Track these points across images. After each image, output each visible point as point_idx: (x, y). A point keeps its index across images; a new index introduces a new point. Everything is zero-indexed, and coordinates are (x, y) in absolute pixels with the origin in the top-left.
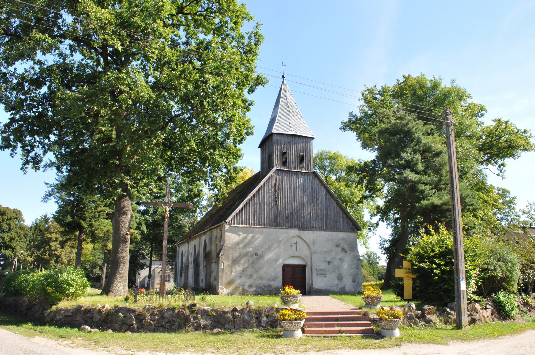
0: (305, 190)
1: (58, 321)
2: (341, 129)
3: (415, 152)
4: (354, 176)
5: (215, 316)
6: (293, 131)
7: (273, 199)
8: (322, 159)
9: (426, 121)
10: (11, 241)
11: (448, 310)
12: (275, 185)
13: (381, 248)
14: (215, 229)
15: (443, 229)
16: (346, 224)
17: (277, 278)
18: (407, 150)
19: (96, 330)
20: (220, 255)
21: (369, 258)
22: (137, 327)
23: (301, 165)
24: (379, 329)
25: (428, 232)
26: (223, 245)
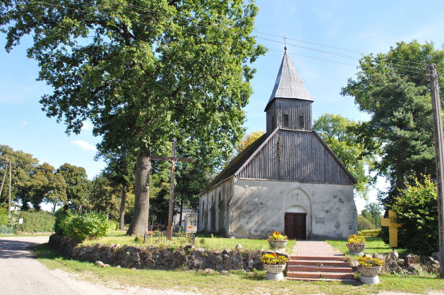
0: (305, 147)
1: (81, 256)
2: (341, 94)
3: (407, 111)
4: (355, 137)
5: (207, 257)
6: (293, 95)
7: (276, 155)
8: (325, 122)
9: (418, 83)
10: (77, 192)
11: (432, 259)
12: (278, 143)
13: (379, 200)
14: (227, 182)
15: (428, 181)
16: (343, 178)
17: (280, 224)
18: (399, 110)
19: (108, 265)
20: (230, 204)
21: (372, 208)
22: (142, 264)
23: (302, 125)
24: (359, 275)
25: (412, 183)
26: (232, 195)
